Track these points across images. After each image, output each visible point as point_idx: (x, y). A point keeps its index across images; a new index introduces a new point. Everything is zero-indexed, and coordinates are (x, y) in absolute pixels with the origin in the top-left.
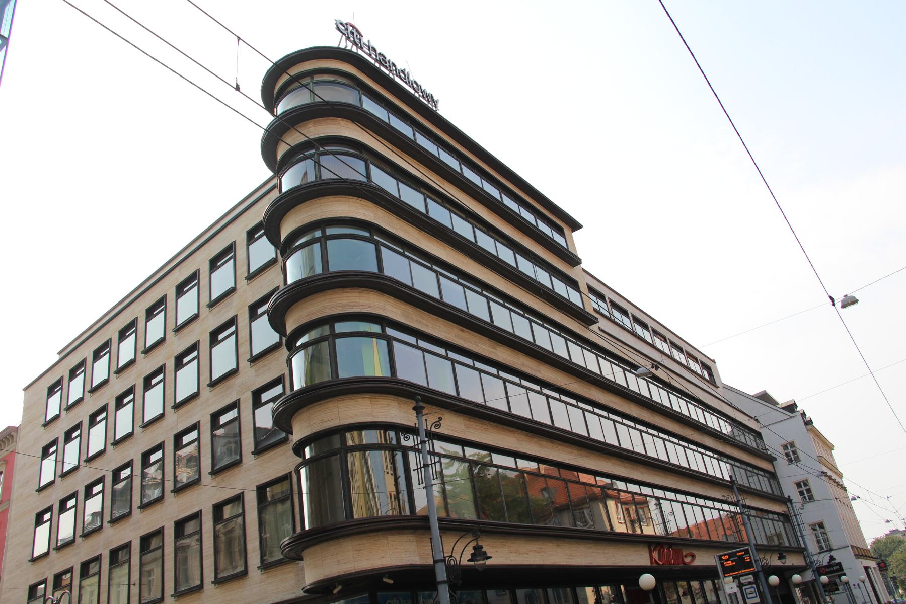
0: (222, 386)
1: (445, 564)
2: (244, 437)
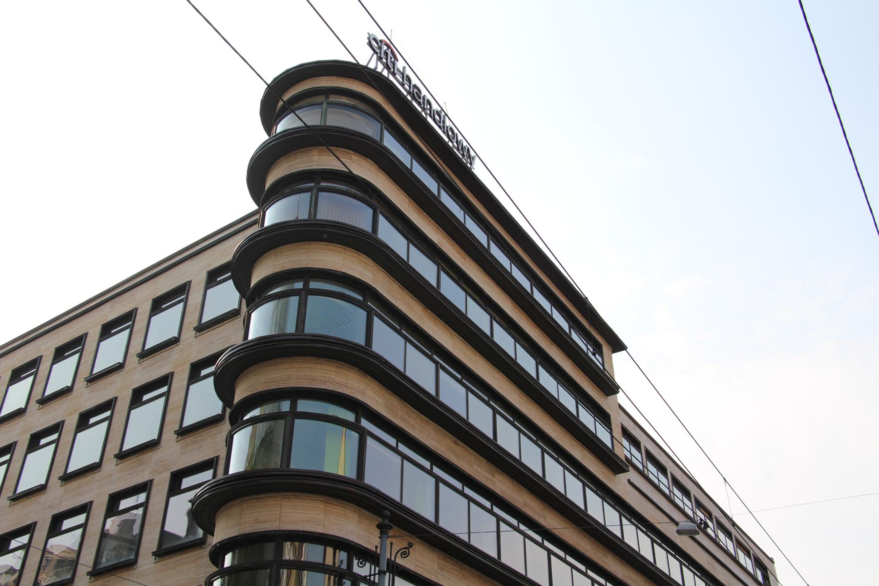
0: (132, 461)
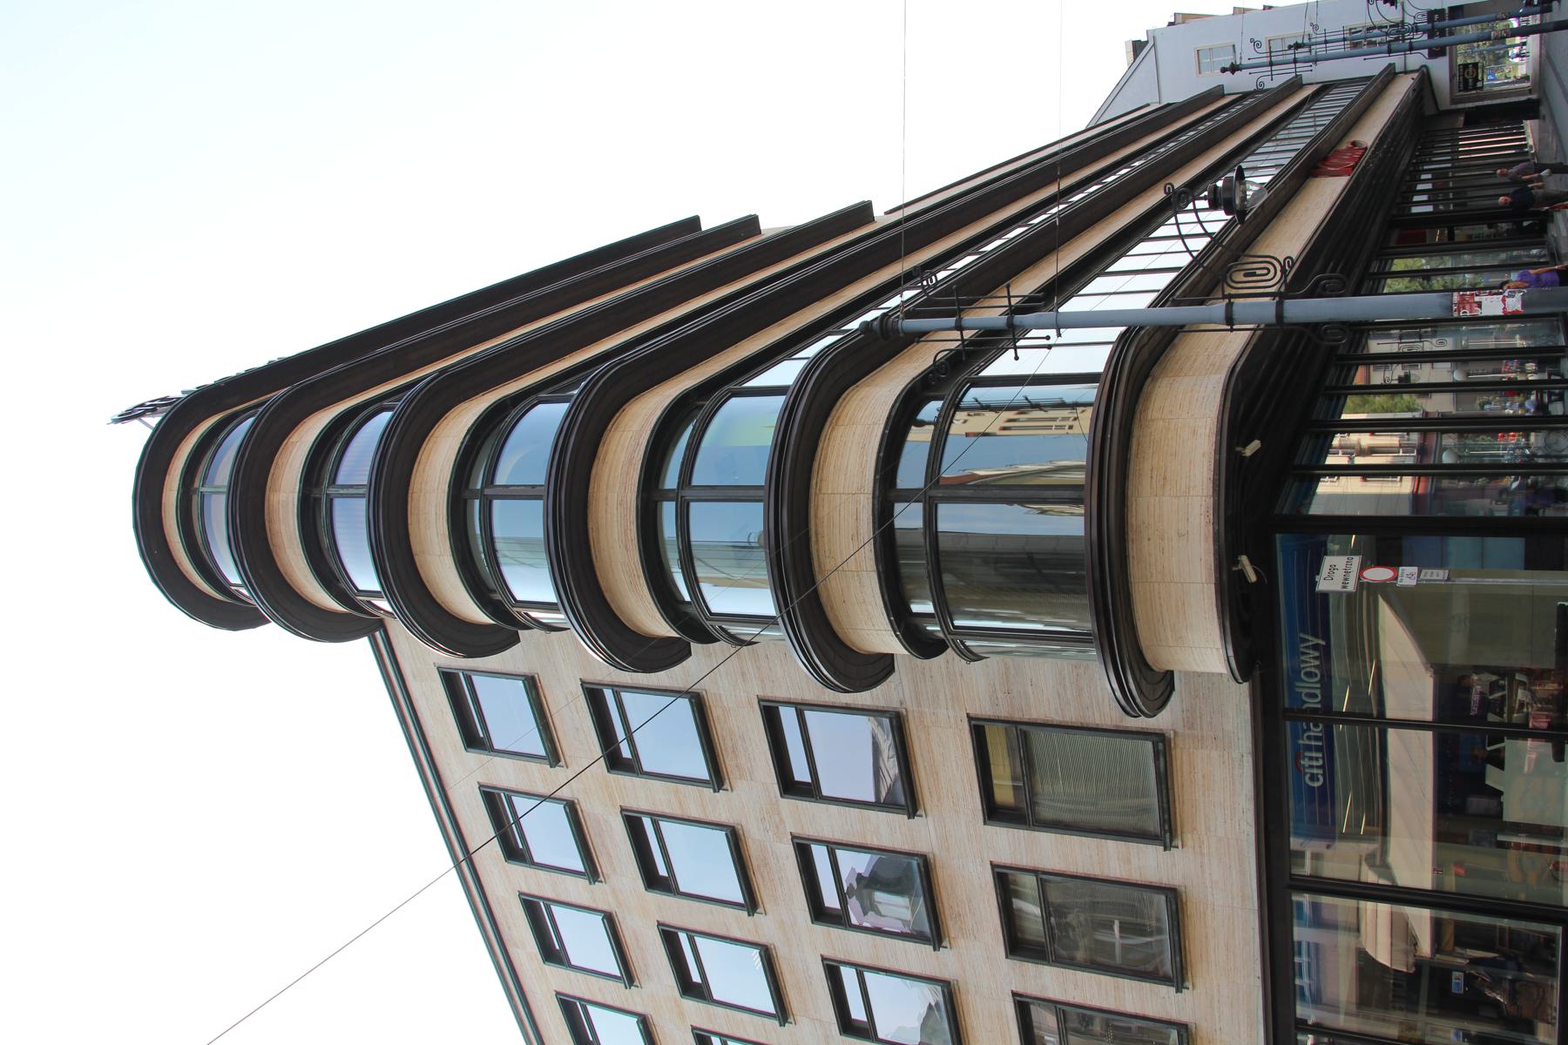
0: (760, 880)
2: (875, 839)
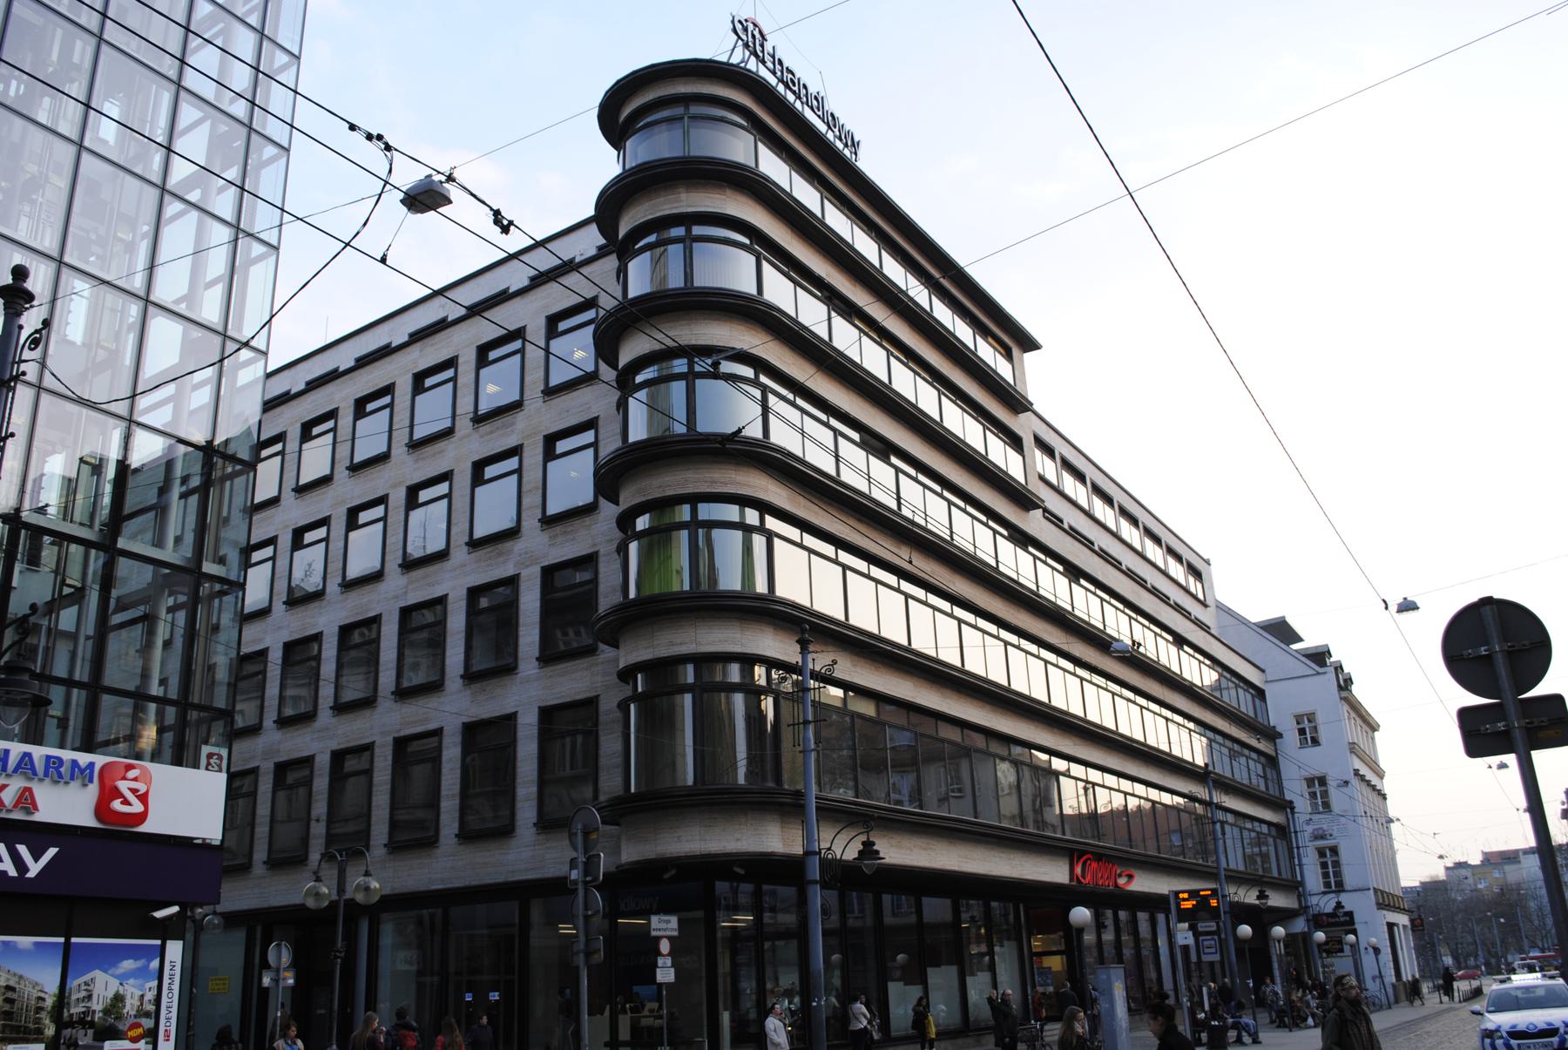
1: (820, 857)
